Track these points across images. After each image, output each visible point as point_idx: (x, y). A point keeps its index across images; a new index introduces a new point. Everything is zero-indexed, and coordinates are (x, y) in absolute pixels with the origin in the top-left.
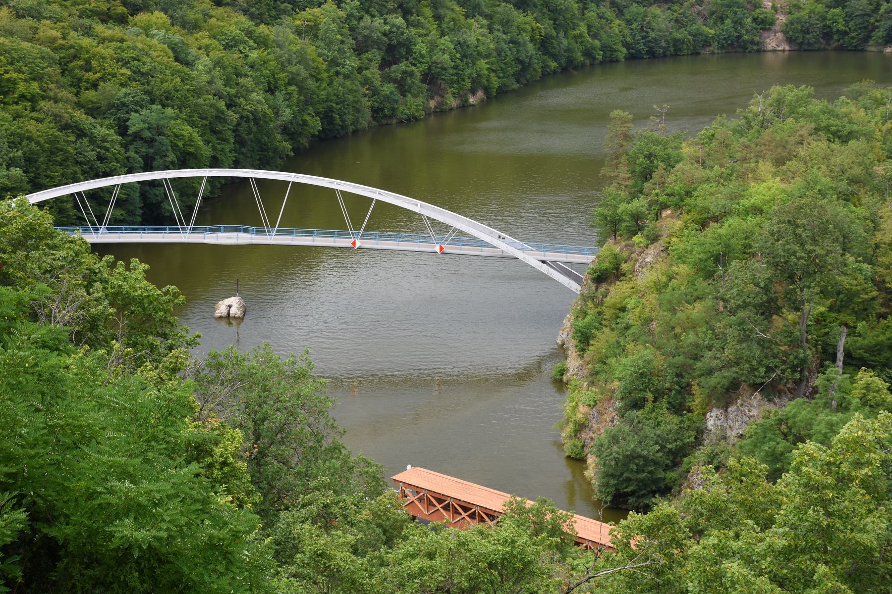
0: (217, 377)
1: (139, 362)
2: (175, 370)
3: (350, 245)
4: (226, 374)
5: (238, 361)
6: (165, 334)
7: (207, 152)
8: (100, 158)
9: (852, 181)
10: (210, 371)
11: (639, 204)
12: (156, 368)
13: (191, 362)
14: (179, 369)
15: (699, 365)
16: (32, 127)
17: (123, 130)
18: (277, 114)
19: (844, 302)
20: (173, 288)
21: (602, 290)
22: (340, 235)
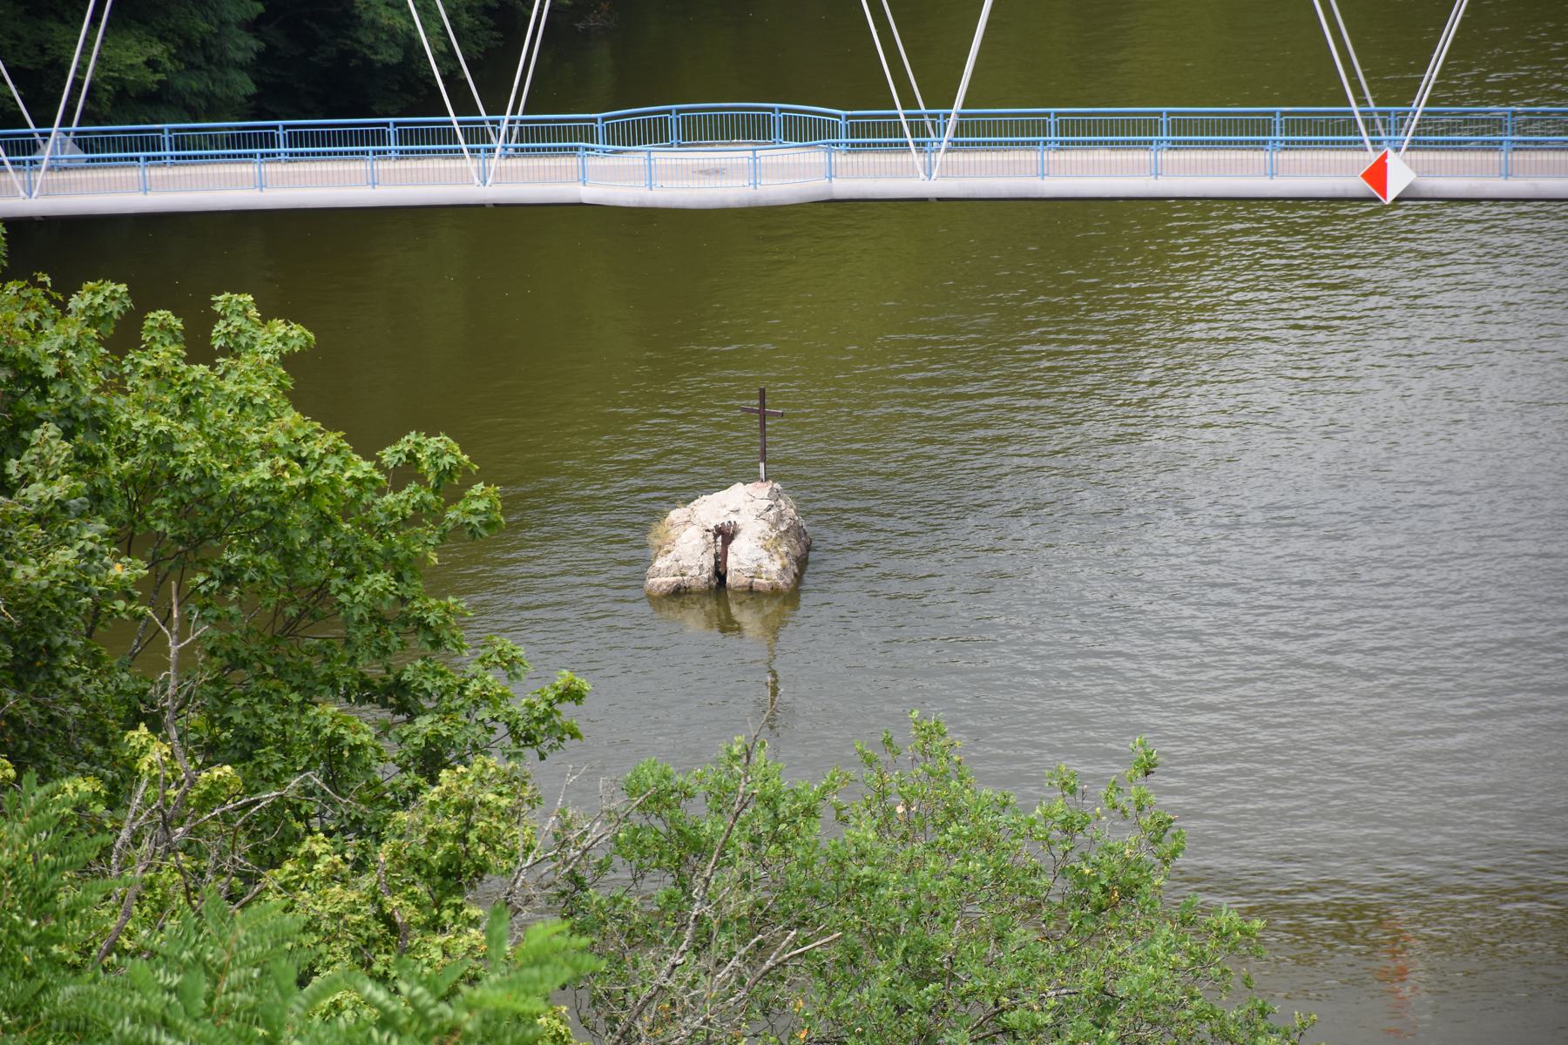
0: (676, 905)
1: (272, 838)
2: (454, 877)
3: (1356, 185)
4: (723, 891)
5: (779, 824)
6: (400, 687)
10: (639, 874)
12: (360, 866)
13: (537, 829)
14: (481, 870)
20: (437, 449)
22: (1306, 132)
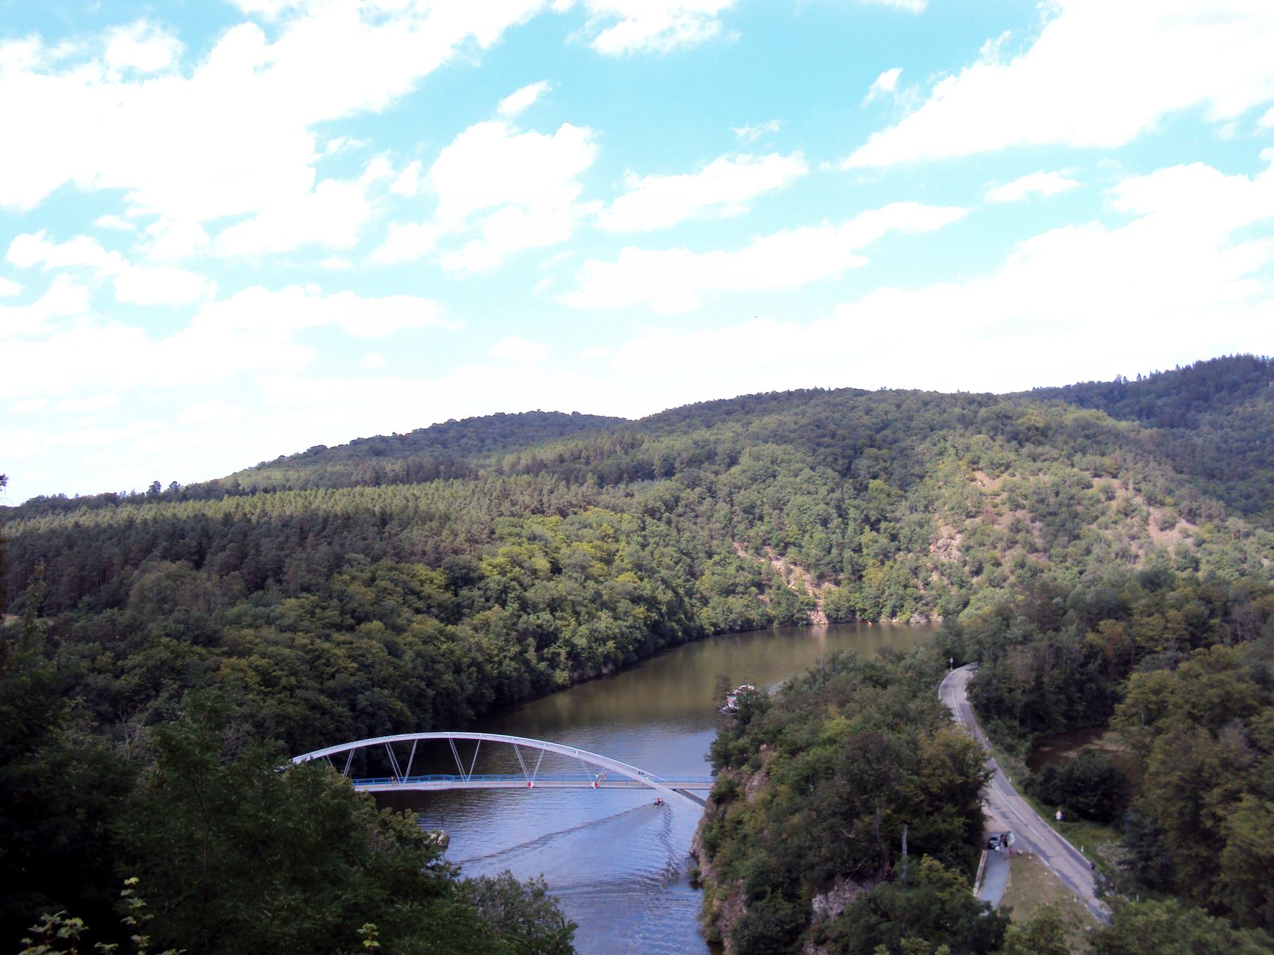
7: (413, 720)
8: (338, 730)
9: (896, 715)
11: (744, 741)
15: (803, 862)
16: (290, 709)
17: (353, 707)
18: (462, 689)
19: (901, 804)
21: (722, 808)
